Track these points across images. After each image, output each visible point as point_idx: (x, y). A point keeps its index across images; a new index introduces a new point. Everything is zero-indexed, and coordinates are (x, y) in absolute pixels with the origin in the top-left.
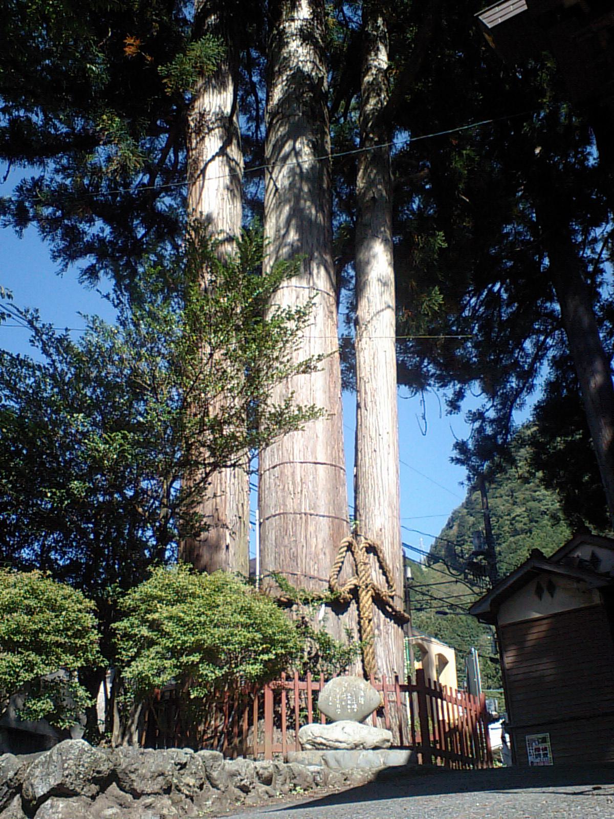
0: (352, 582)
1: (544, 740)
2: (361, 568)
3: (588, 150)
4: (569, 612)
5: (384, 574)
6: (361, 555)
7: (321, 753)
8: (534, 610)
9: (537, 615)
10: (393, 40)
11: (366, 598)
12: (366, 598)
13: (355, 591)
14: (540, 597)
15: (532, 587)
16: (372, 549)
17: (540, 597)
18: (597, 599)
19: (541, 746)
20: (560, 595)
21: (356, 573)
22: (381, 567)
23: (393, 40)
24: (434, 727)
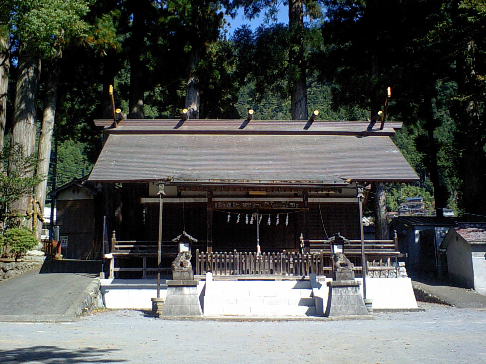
0: (33, 212)
1: (66, 238)
2: (35, 208)
3: (342, 110)
4: (83, 200)
5: (40, 209)
6: (35, 204)
7: (30, 257)
8: (71, 197)
9: (71, 199)
10: (234, 218)
11: (36, 216)
12: (36, 216)
13: (33, 215)
14: (74, 193)
15: (72, 189)
16: (38, 203)
17: (74, 193)
18: (92, 198)
19: (65, 240)
20: (80, 194)
21: (33, 209)
22: (40, 207)
23: (234, 218)
24: (95, 355)
